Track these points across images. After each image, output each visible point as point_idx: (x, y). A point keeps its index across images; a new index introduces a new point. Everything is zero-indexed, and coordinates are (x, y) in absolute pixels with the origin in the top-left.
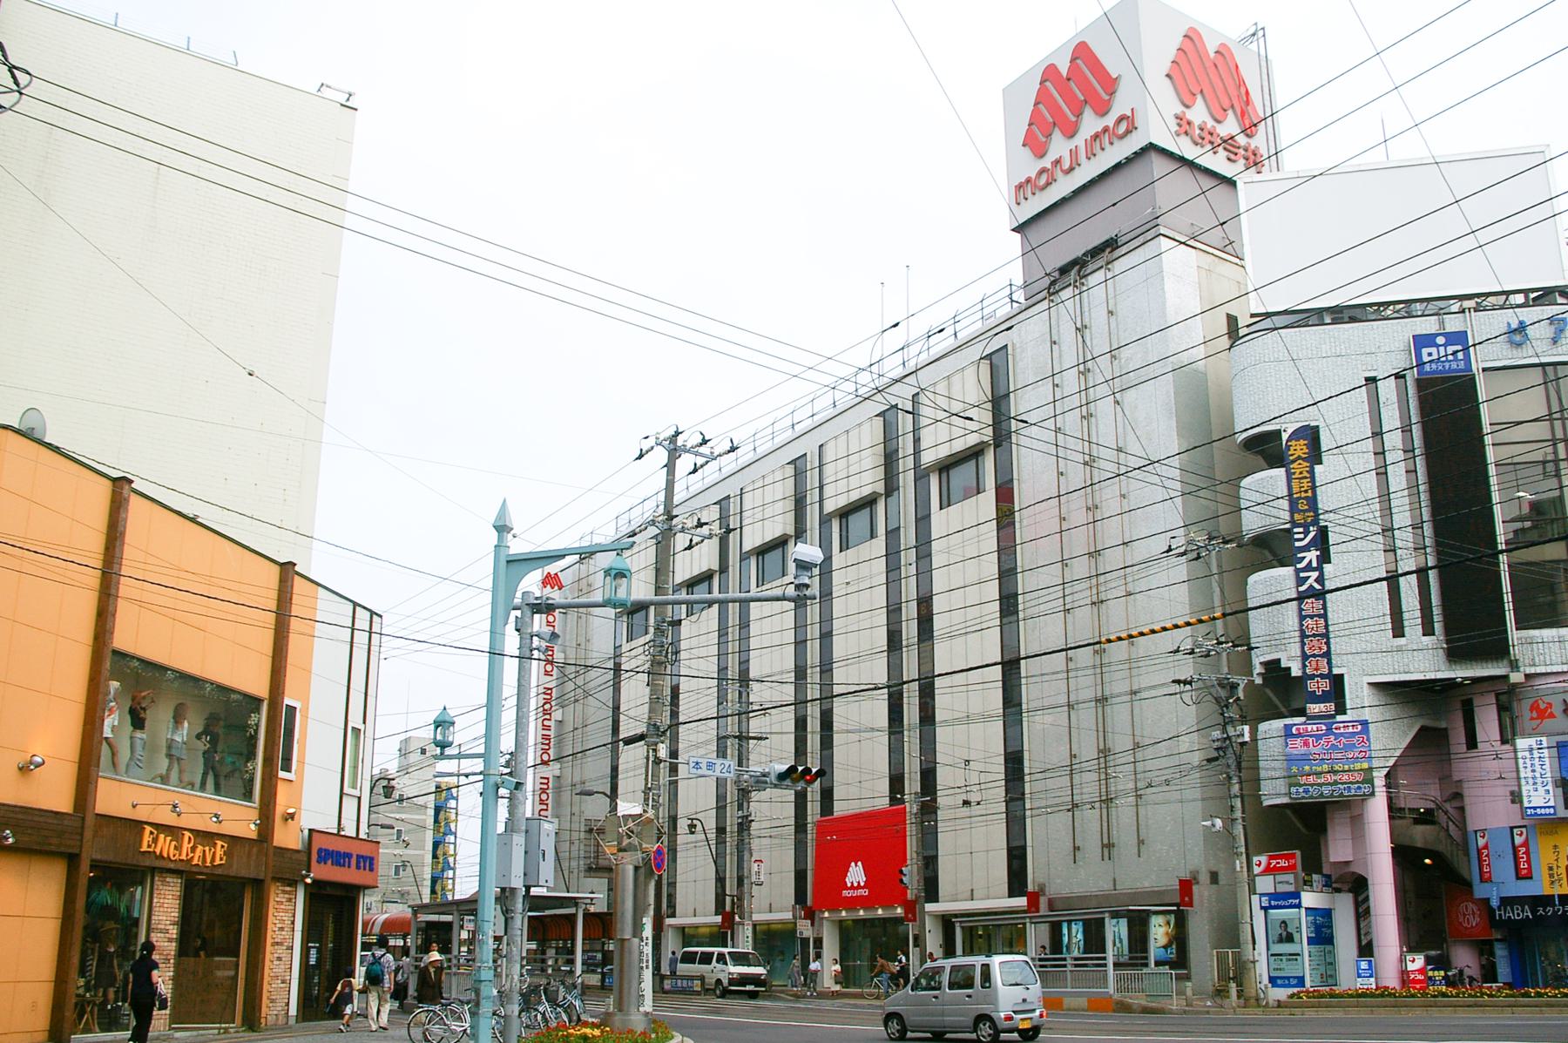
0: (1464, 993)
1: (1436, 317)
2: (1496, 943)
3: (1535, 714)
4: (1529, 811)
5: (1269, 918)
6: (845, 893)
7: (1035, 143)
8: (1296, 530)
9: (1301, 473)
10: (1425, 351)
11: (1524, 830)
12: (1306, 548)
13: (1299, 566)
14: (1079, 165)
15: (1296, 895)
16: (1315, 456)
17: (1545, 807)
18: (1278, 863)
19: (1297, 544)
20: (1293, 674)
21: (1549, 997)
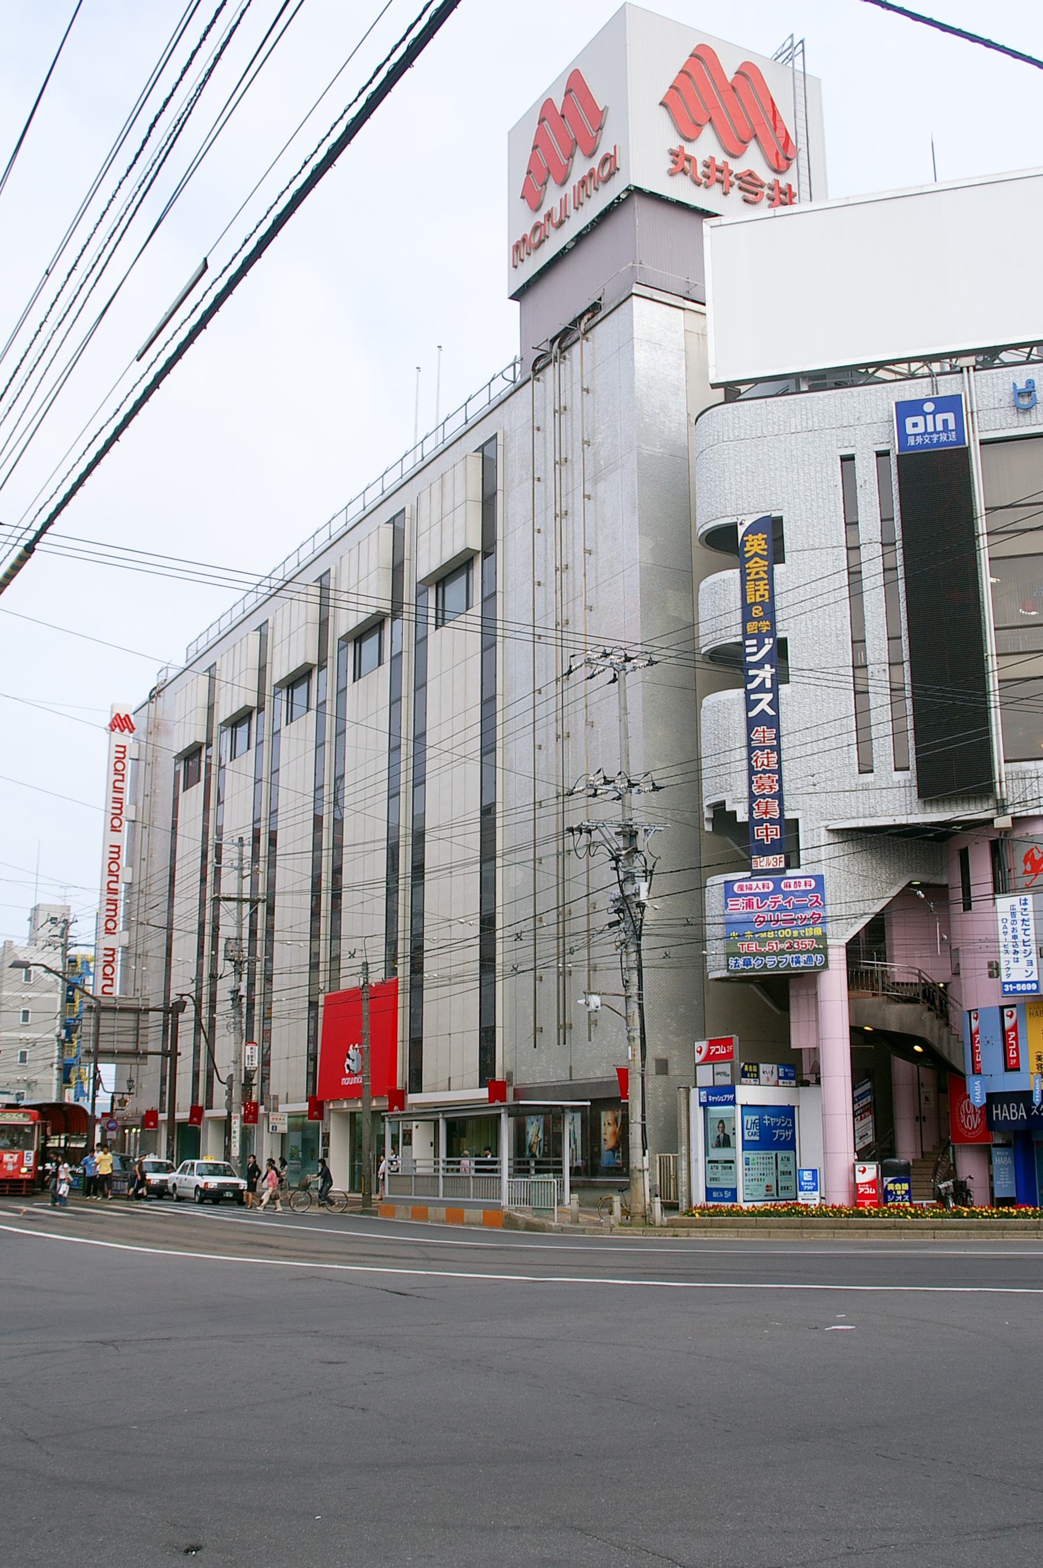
0: (884, 1212)
1: (929, 379)
2: (993, 1149)
3: (1029, 867)
4: (1007, 988)
5: (710, 1116)
6: (345, 1081)
7: (532, 197)
8: (748, 643)
9: (757, 573)
10: (909, 421)
11: (1014, 1010)
12: (759, 665)
13: (750, 686)
14: (569, 217)
15: (731, 1089)
16: (777, 554)
17: (1026, 982)
18: (717, 1050)
19: (749, 659)
20: (739, 820)
21: (983, 1217)
